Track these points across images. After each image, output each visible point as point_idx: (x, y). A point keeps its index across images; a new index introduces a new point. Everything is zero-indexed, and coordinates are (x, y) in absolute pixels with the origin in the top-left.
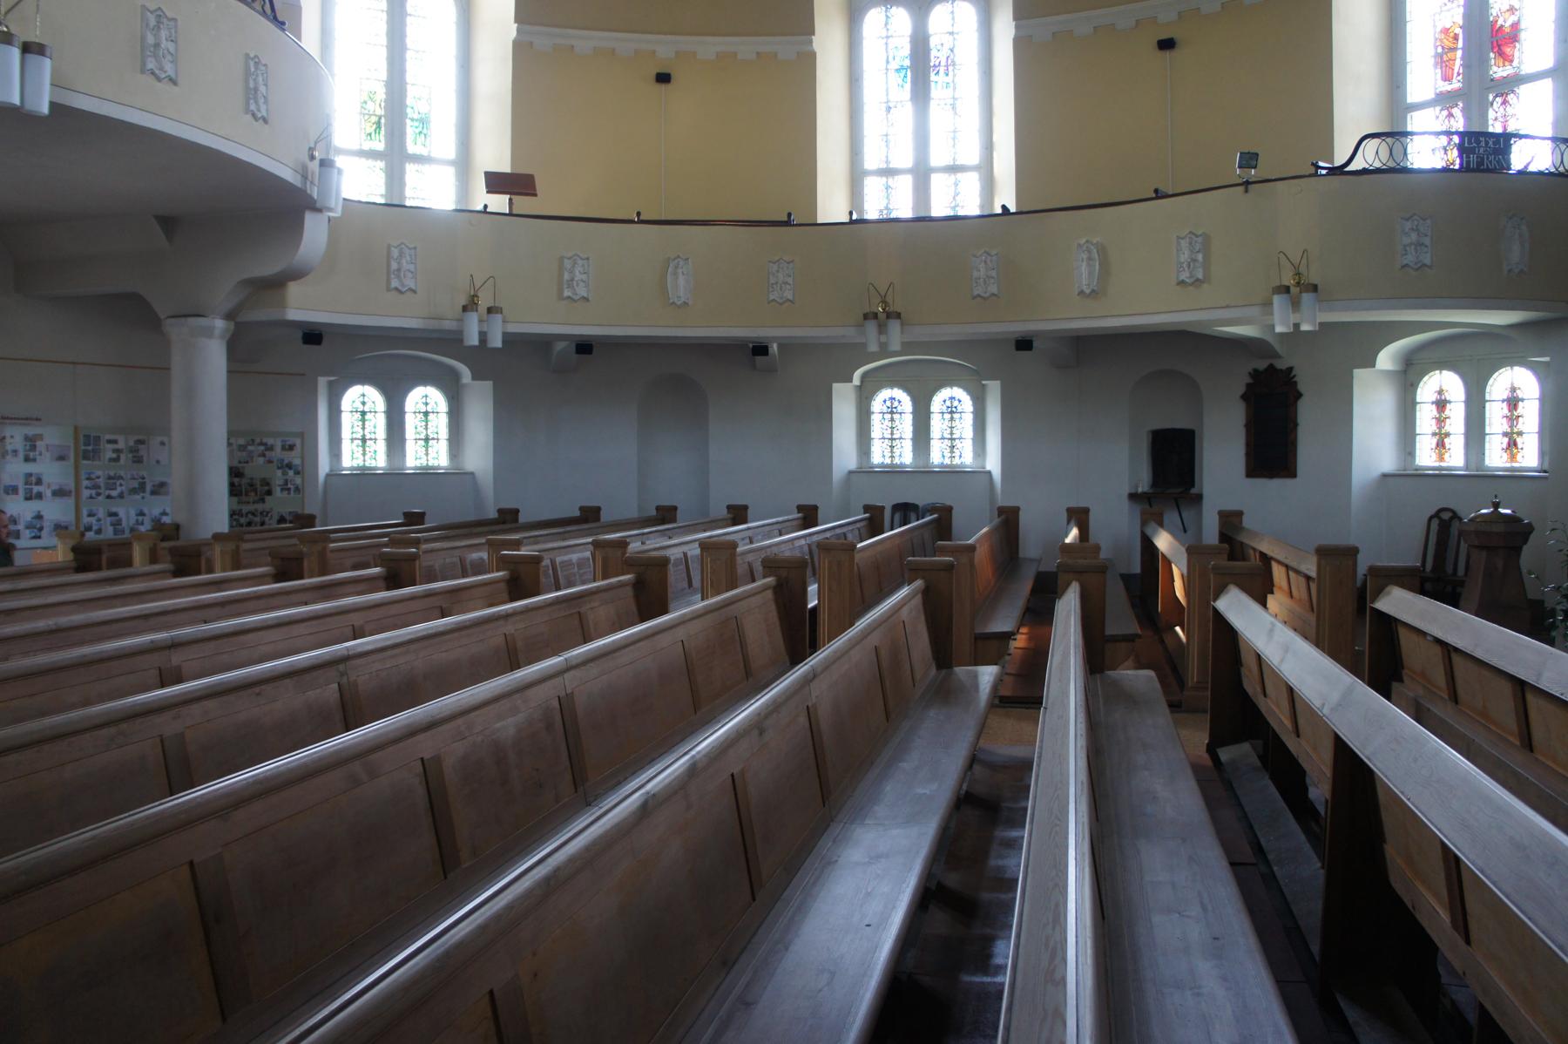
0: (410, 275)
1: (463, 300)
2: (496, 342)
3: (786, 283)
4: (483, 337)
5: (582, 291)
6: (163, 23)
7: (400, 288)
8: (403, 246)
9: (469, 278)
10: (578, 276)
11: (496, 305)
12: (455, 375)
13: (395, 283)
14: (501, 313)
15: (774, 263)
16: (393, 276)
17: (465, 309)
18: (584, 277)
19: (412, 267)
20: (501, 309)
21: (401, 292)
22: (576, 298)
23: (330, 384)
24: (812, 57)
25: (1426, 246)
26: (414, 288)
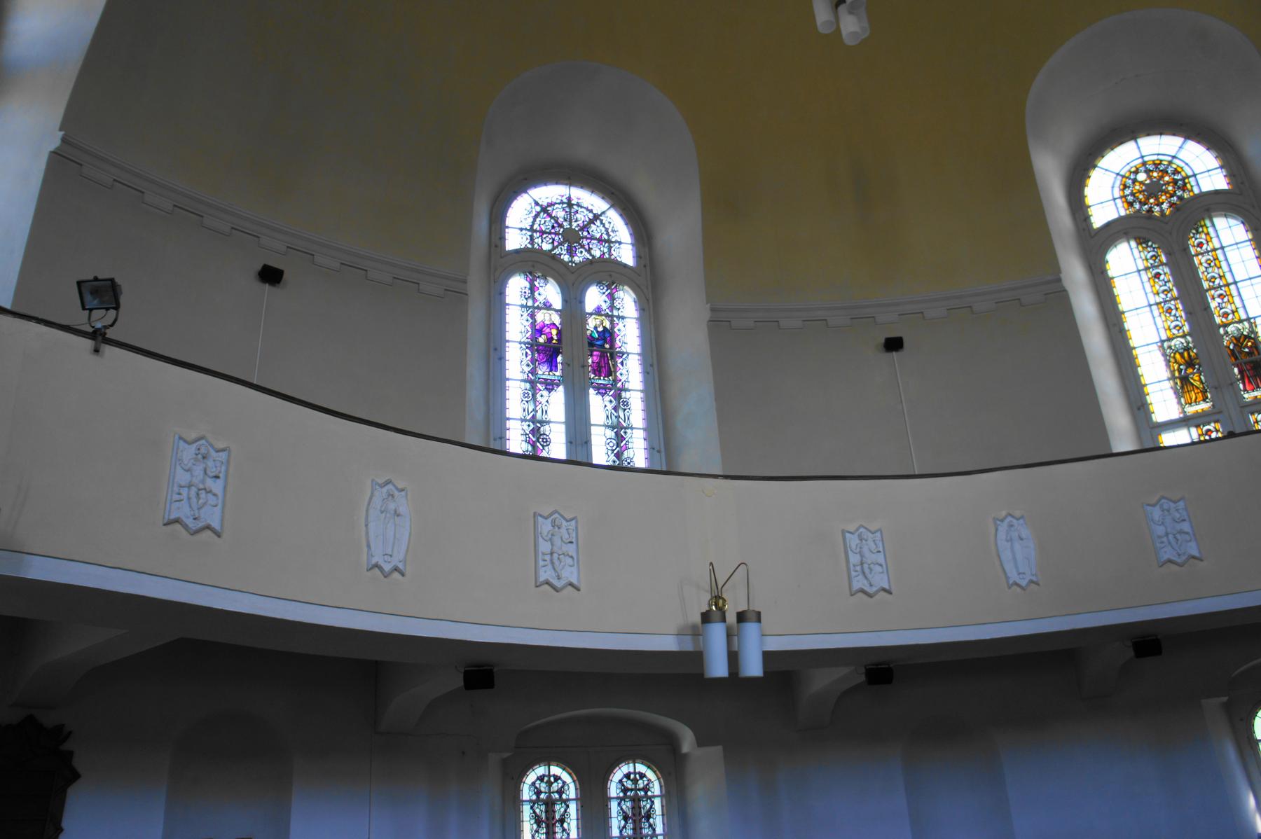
0: (878, 569)
1: (702, 603)
2: (753, 667)
3: (1181, 532)
4: (734, 658)
5: (881, 581)
6: (1219, 284)
7: (867, 588)
8: (862, 530)
9: (708, 567)
10: (870, 558)
11: (751, 608)
12: (672, 742)
13: (858, 583)
14: (759, 620)
15: (1153, 505)
16: (853, 574)
17: (706, 618)
18: (880, 558)
19: (880, 558)
20: (759, 614)
21: (870, 596)
22: (871, 590)
23: (505, 763)
24: (1064, 291)
25: (215, 495)
26: (887, 587)
